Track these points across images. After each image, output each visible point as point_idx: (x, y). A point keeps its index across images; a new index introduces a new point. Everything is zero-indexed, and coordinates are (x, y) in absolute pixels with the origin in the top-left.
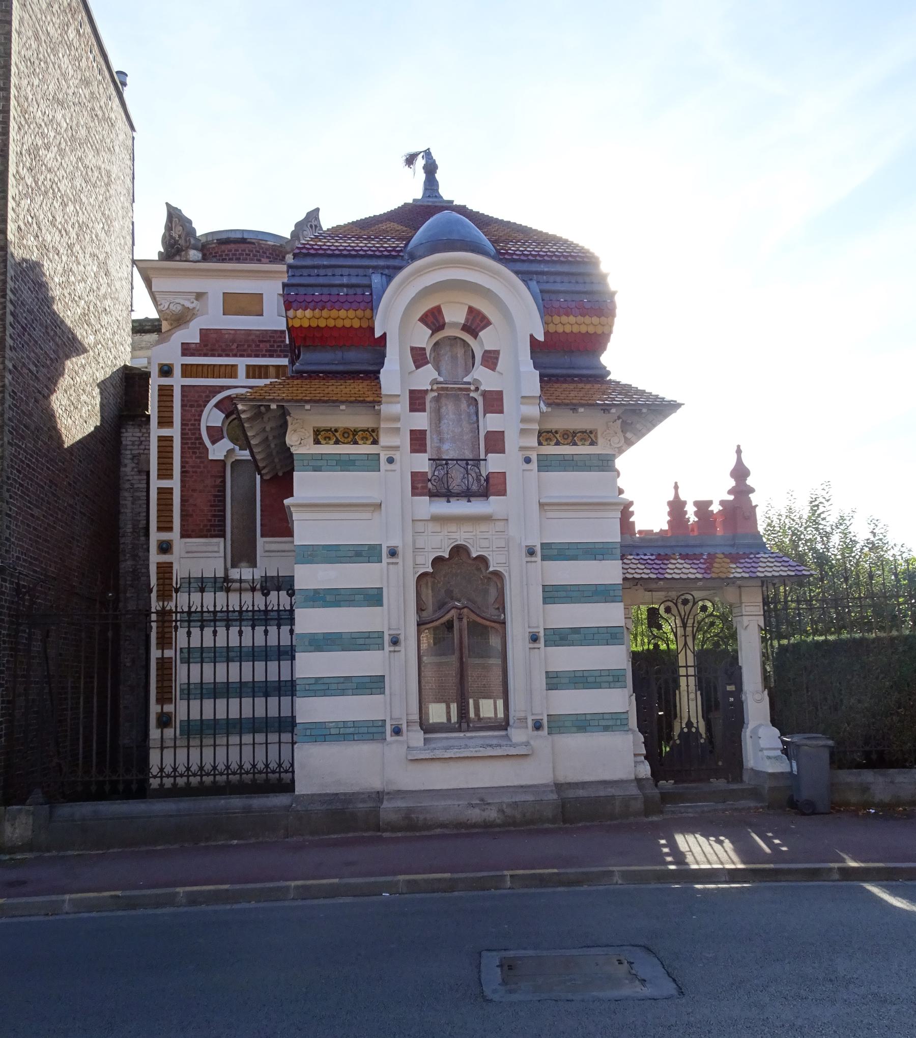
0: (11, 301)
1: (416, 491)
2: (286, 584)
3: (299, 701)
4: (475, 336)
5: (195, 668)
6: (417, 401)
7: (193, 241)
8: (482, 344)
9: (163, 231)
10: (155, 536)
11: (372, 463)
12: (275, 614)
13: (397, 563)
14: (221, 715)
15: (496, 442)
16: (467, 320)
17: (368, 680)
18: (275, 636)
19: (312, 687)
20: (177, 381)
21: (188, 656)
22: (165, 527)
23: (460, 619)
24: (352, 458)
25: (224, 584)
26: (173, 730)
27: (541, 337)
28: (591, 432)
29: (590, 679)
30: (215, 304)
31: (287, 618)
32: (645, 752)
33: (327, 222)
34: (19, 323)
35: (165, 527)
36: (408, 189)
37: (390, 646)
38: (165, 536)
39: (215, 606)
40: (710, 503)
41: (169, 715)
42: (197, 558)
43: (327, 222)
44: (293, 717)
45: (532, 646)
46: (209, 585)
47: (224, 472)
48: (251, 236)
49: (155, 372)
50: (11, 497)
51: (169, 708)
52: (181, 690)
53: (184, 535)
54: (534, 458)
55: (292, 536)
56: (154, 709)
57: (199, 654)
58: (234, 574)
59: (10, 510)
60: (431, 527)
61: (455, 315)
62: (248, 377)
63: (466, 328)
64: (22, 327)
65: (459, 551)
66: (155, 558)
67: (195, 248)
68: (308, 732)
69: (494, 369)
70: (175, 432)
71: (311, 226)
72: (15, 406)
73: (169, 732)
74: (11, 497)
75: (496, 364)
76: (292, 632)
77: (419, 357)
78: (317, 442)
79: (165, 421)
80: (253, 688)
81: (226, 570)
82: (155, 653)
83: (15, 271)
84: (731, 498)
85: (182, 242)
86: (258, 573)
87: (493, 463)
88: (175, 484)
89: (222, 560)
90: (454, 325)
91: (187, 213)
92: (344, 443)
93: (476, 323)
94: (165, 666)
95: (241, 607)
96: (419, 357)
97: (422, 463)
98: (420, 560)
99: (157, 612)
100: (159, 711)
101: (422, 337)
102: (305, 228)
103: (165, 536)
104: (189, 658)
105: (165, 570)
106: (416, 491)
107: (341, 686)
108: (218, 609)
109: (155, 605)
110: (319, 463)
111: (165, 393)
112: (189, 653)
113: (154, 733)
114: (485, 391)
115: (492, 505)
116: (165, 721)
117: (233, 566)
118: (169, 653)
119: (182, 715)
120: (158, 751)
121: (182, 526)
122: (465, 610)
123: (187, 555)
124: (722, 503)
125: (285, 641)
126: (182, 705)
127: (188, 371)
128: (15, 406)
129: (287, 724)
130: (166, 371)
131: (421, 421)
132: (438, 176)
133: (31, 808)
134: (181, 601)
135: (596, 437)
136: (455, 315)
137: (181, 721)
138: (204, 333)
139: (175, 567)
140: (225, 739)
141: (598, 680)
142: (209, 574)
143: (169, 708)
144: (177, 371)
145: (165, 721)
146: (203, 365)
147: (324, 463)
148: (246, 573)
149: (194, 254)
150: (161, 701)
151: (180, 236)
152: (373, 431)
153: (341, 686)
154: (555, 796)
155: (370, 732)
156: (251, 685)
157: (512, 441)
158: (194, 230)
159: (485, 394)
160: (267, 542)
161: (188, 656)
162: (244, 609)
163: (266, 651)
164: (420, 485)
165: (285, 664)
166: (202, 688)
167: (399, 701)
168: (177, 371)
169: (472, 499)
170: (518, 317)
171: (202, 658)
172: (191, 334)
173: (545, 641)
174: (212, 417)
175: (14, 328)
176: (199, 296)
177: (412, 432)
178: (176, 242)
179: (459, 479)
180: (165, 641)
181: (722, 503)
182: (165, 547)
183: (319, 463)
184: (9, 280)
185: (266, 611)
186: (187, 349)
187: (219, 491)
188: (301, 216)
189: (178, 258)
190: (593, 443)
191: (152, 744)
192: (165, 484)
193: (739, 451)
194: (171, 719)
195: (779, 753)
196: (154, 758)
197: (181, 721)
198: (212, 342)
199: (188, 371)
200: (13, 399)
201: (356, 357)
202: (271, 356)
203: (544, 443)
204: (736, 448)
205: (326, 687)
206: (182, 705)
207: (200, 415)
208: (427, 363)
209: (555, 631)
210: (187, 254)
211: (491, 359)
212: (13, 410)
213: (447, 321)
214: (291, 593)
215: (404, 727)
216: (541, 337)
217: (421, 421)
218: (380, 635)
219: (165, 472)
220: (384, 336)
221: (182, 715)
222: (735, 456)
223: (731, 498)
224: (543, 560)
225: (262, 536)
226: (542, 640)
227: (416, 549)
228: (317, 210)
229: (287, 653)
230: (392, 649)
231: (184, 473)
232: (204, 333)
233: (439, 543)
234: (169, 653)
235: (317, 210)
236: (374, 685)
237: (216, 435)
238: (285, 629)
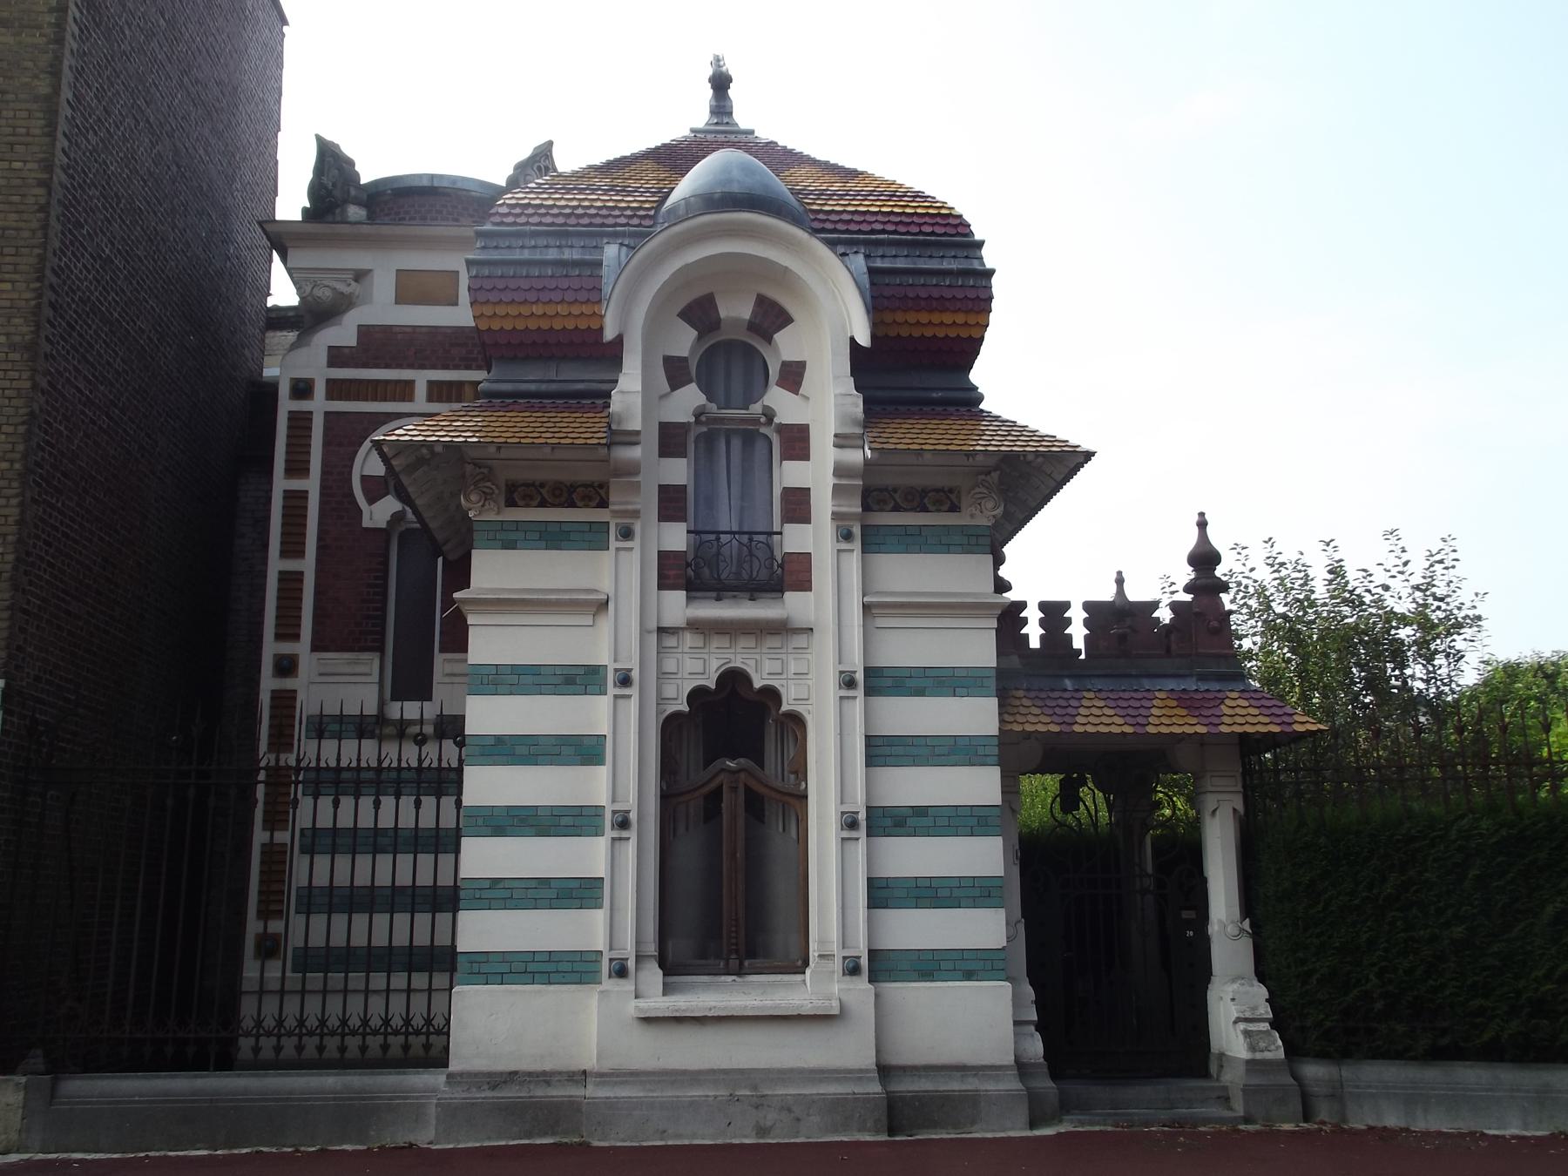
0: (52, 287)
1: (665, 582)
2: (451, 728)
3: (464, 917)
4: (768, 339)
5: (322, 862)
6: (671, 440)
7: (353, 192)
8: (776, 351)
9: (310, 176)
10: (270, 648)
11: (594, 538)
12: (413, 775)
13: (629, 697)
14: (359, 940)
15: (797, 505)
16: (754, 313)
17: (576, 884)
18: (430, 813)
19: (486, 894)
20: (319, 405)
21: (315, 841)
22: (287, 630)
23: (734, 789)
24: (565, 528)
25: (364, 727)
26: (280, 963)
27: (864, 340)
28: (951, 491)
29: (943, 893)
30: (383, 286)
31: (447, 782)
32: (1035, 1018)
33: (567, 161)
34: (62, 317)
35: (287, 630)
36: (688, 114)
37: (613, 828)
38: (287, 648)
39: (339, 760)
40: (1155, 605)
41: (275, 938)
42: (338, 684)
43: (567, 161)
44: (454, 946)
45: (846, 834)
46: (351, 727)
47: (387, 549)
48: (445, 184)
49: (284, 390)
50: (31, 583)
51: (276, 926)
52: (298, 897)
53: (316, 647)
54: (857, 530)
55: (466, 650)
56: (253, 926)
57: (329, 841)
58: (394, 710)
59: (29, 602)
60: (689, 639)
61: (736, 309)
62: (430, 399)
63: (753, 327)
64: (69, 324)
65: (733, 679)
66: (268, 683)
67: (359, 203)
68: (476, 967)
69: (797, 393)
70: (312, 485)
71: (539, 168)
72: (48, 443)
73: (274, 971)
74: (31, 583)
75: (800, 384)
76: (459, 803)
77: (676, 372)
78: (511, 503)
79: (297, 467)
80: (414, 895)
81: (382, 704)
82: (260, 836)
83: (63, 243)
84: (1188, 598)
85: (337, 193)
86: (430, 710)
87: (795, 539)
88: (308, 565)
89: (376, 688)
90: (736, 322)
91: (348, 150)
92: (554, 506)
93: (771, 317)
94: (276, 858)
95: (380, 762)
96: (676, 372)
97: (676, 537)
98: (670, 691)
99: (267, 768)
100: (261, 930)
101: (683, 340)
102: (529, 171)
103: (287, 648)
104: (313, 844)
105: (285, 702)
106: (665, 582)
107: (531, 893)
108: (344, 764)
109: (265, 757)
110: (513, 536)
111: (300, 423)
112: (314, 836)
113: (250, 970)
114: (781, 425)
115: (794, 605)
116: (269, 948)
117: (394, 699)
118: (282, 837)
119: (296, 940)
120: (255, 998)
121: (315, 632)
122: (742, 775)
123: (447, 680)
124: (1175, 607)
125: (448, 821)
126: (297, 921)
127: (336, 389)
128: (48, 443)
129: (443, 961)
130: (302, 389)
131: (678, 471)
132: (732, 92)
133: (23, 1080)
134: (308, 750)
135: (959, 498)
136: (736, 309)
137: (295, 949)
138: (365, 332)
139: (301, 697)
140: (385, 981)
141: (956, 893)
142: (352, 709)
143: (276, 926)
144: (320, 389)
145: (269, 948)
146: (378, 381)
147: (520, 535)
148: (411, 710)
149: (355, 212)
150: (265, 914)
151: (334, 185)
152: (601, 486)
153: (531, 893)
154: (875, 1088)
155: (570, 968)
156: (410, 891)
157: (823, 504)
158: (357, 175)
159: (783, 429)
160: (449, 661)
161: (315, 841)
162: (385, 765)
163: (437, 836)
164: (675, 572)
165: (446, 860)
166: (331, 896)
167: (618, 923)
168: (320, 389)
169: (756, 594)
170: (834, 311)
171: (334, 844)
172: (343, 333)
173: (868, 827)
174: (368, 464)
175: (53, 326)
176: (360, 276)
177: (663, 489)
178: (329, 193)
179: (733, 566)
180: (276, 819)
181: (1175, 607)
182: (286, 667)
183: (513, 536)
184: (50, 254)
185: (379, 770)
186: (337, 357)
187: (377, 578)
188: (525, 153)
189: (330, 218)
190: (954, 508)
191: (245, 987)
192: (291, 565)
193: (1202, 524)
194: (278, 945)
195: (1265, 1026)
196: (248, 1007)
197: (295, 949)
198: (379, 345)
199: (336, 389)
200: (46, 432)
201: (576, 376)
202: (468, 368)
203: (875, 507)
204: (1196, 518)
205: (507, 894)
206: (297, 921)
207: (352, 460)
208: (690, 381)
209: (886, 810)
210: (344, 212)
211: (793, 376)
212: (43, 450)
213: (723, 313)
214: (460, 738)
215: (631, 964)
216: (864, 340)
217: (678, 471)
218: (597, 811)
219: (293, 547)
220: (619, 342)
221: (296, 940)
222: (1196, 530)
223: (1188, 598)
224: (867, 694)
225: (441, 651)
226: (863, 824)
227: (662, 675)
228: (550, 143)
229: (446, 842)
230: (616, 834)
231: (322, 547)
232: (365, 332)
233: (698, 667)
234: (282, 837)
235: (550, 143)
236: (579, 893)
237: (375, 490)
238: (448, 802)
